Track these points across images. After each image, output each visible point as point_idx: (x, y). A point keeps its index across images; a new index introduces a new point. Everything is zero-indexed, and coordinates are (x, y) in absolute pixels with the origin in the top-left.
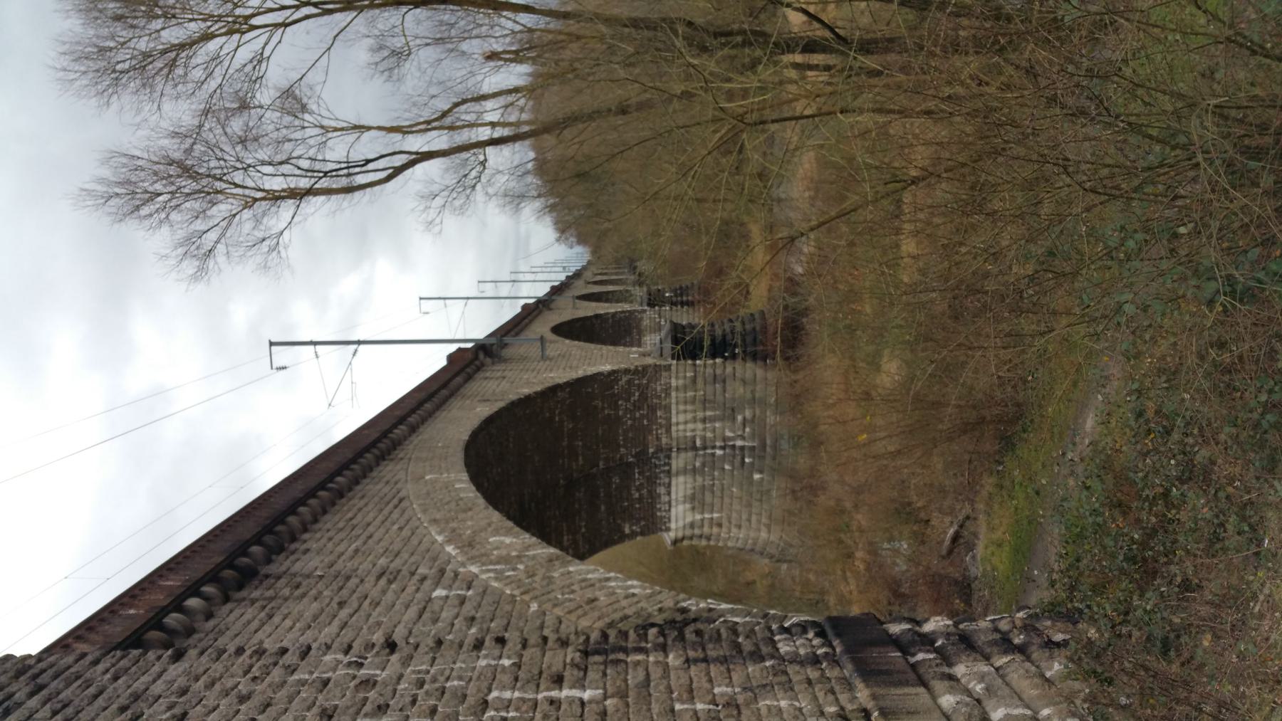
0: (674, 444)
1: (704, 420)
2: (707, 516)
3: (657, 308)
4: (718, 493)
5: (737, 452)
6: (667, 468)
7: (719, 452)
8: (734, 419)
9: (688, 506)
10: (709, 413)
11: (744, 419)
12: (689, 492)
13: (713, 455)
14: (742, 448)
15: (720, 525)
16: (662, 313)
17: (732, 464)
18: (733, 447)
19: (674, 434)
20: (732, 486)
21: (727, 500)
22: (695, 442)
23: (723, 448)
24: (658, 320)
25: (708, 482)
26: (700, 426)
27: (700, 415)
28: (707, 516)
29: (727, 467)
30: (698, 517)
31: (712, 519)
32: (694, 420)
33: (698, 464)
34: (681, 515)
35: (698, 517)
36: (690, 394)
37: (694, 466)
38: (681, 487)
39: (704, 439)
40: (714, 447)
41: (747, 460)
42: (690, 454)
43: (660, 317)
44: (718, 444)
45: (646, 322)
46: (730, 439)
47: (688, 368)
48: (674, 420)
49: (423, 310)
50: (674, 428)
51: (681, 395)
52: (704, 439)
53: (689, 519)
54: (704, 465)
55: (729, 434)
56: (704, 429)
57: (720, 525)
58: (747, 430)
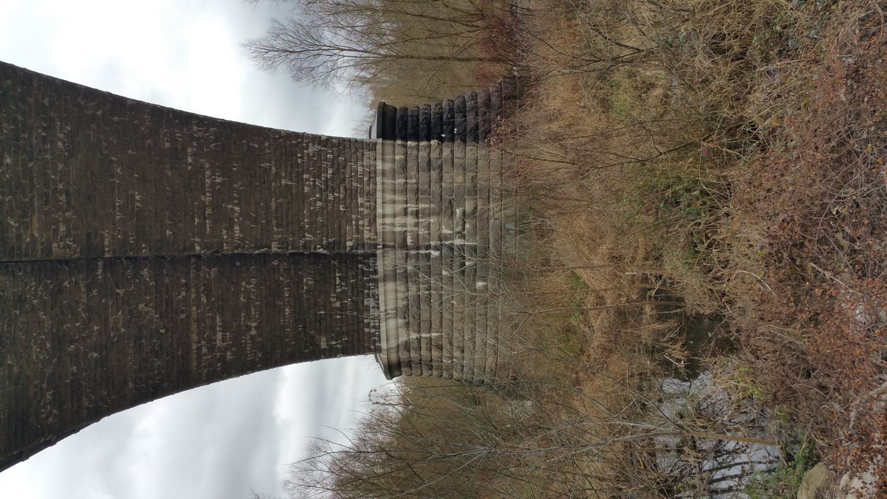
1: (417, 214)
7: (435, 253)
8: (452, 214)
9: (401, 321)
11: (464, 213)
12: (401, 304)
13: (428, 256)
15: (440, 348)
18: (451, 248)
19: (379, 228)
22: (405, 239)
26: (411, 220)
27: (412, 207)
28: (424, 335)
34: (392, 332)
39: (417, 237)
42: (400, 253)
44: (432, 243)
46: (447, 237)
48: (379, 211)
50: (379, 221)
52: (417, 237)
53: (403, 339)
55: (446, 231)
56: (417, 225)
57: (440, 348)
58: (467, 226)
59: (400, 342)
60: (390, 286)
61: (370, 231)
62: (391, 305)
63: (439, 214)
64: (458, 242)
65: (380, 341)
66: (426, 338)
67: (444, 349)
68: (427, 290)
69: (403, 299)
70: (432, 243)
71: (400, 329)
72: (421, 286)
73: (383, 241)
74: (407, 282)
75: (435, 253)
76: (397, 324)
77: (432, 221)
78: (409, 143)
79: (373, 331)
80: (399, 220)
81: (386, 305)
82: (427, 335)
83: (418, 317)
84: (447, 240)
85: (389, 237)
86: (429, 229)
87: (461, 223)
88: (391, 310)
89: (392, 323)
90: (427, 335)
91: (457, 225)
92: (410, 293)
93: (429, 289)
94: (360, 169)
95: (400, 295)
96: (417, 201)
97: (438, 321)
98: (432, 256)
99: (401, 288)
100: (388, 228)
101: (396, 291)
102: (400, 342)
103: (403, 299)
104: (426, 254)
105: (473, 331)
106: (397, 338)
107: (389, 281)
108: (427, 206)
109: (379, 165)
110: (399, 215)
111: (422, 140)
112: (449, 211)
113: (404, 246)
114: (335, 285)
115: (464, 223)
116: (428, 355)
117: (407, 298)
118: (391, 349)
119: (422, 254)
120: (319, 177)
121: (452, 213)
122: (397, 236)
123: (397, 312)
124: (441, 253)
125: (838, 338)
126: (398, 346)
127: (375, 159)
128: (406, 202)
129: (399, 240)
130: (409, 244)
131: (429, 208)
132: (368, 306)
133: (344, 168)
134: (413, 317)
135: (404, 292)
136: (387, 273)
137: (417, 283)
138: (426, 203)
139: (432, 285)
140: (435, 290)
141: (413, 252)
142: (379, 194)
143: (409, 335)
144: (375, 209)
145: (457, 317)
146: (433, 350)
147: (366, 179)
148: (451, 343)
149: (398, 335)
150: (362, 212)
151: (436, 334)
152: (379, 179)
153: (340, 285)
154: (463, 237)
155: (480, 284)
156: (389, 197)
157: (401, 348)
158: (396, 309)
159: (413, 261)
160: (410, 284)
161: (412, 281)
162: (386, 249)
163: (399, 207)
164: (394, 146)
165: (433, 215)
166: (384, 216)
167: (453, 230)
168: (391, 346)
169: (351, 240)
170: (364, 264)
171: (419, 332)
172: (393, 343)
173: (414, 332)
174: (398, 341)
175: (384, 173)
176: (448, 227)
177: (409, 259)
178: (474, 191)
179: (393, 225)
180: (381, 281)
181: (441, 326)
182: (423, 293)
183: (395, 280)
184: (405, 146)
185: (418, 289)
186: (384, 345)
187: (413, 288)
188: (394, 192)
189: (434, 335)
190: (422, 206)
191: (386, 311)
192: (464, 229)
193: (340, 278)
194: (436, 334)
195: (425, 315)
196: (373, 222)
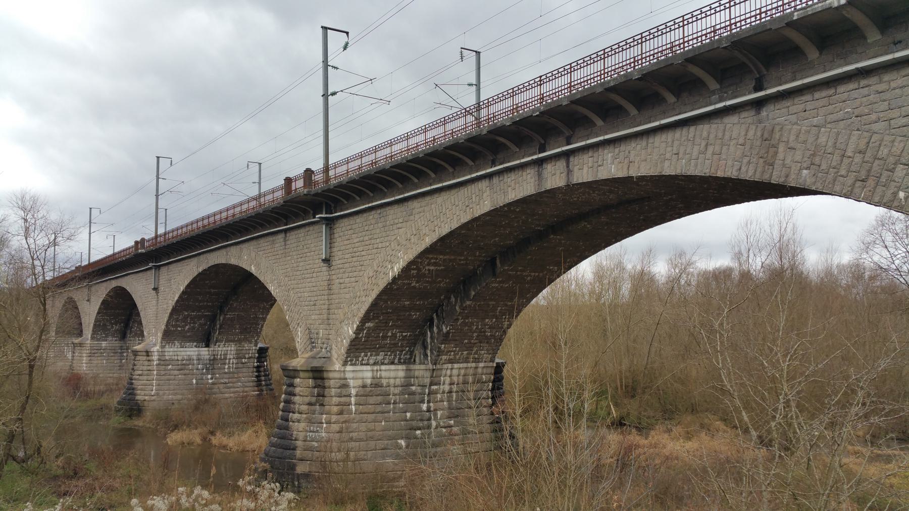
0: (438, 366)
1: (450, 392)
2: (353, 400)
3: (257, 355)
4: (379, 409)
5: (426, 423)
6: (396, 361)
7: (424, 407)
8: (449, 418)
9: (369, 381)
10: (454, 395)
11: (451, 427)
12: (384, 382)
13: (422, 402)
14: (429, 427)
15: (341, 413)
16: (252, 360)
17: (412, 419)
18: (429, 419)
19: (445, 366)
20: (386, 421)
21: (371, 417)
22: (436, 384)
23: (429, 410)
24: (247, 356)
25: (392, 398)
26: (447, 388)
27: (455, 388)
28: (353, 400)
29: (408, 415)
30: (353, 392)
31: (350, 404)
32: (451, 384)
33: (413, 388)
34: (360, 375)
35: (353, 392)
36: (471, 379)
37: (413, 385)
38: (392, 374)
39: (436, 392)
40: (429, 402)
41: (418, 432)
42: (427, 381)
43: (249, 358)
44: (431, 404)
45: (246, 346)
46: (435, 415)
47: (488, 376)
48: (456, 366)
49: (251, 165)
50: (450, 366)
51: (471, 371)
52: (436, 392)
53: (351, 383)
54: (413, 393)
55: (439, 413)
56: (443, 392)
57: (341, 413)
58: (444, 430)
59: (349, 380)
60: (401, 374)
61: (445, 360)
62: (384, 374)
63: (450, 408)
64: (434, 423)
65: (352, 365)
66: (351, 401)
67: (339, 416)
68: (394, 401)
69: (388, 383)
70: (431, 404)
71: (361, 380)
72: (398, 397)
73: (438, 369)
74: (401, 386)
75: (424, 407)
76: (366, 378)
77: (445, 403)
78: (491, 384)
79: (360, 359)
80: (448, 380)
81: (385, 370)
82: (353, 403)
83: (370, 394)
84: (434, 415)
85: (439, 373)
86: (440, 401)
87: (446, 425)
88: (380, 374)
89: (369, 375)
90: (353, 403)
91: (444, 422)
92: (392, 389)
93: (395, 403)
94: (483, 352)
95: (392, 381)
96: (457, 392)
97: (366, 410)
98: (422, 404)
99: (398, 382)
100: (444, 372)
101: (395, 378)
102: (349, 380)
103: (388, 383)
104: (424, 400)
105: (360, 440)
106: (353, 378)
107: (406, 373)
108: (454, 399)
109: (481, 365)
110: (451, 379)
111: (492, 393)
112: (452, 415)
113: (431, 384)
114: (402, 332)
115: (445, 427)
116: (333, 403)
117: (389, 386)
118: (345, 374)
119: (424, 397)
120: (489, 328)
121: (450, 418)
122: (438, 379)
123: (377, 378)
124: (424, 411)
125: (883, 460)
126: (346, 379)
127: (485, 362)
128: (458, 384)
129: (436, 380)
130: (432, 387)
131: (453, 401)
132: (378, 355)
133: (487, 343)
134: (371, 391)
135: (395, 384)
136: (413, 371)
137: (402, 393)
138: (456, 399)
139: (397, 405)
140: (394, 408)
141: (427, 391)
142: (465, 365)
143: (354, 387)
144: (458, 363)
145: (371, 426)
146: (338, 407)
147: (476, 356)
148: (345, 422)
149: (356, 379)
150: (458, 354)
151: (354, 409)
152: (474, 365)
153: (402, 335)
154: (437, 427)
155: (402, 442)
156: (463, 372)
157: (342, 382)
158: (381, 378)
159: (420, 391)
160: (400, 389)
161: (403, 390)
162: (431, 371)
163: (455, 379)
164: (490, 374)
165: (449, 404)
166: (452, 369)
167: (440, 419)
168: (346, 373)
169: (445, 347)
170: (407, 352)
171: (356, 396)
172: (349, 375)
173: (357, 392)
174: (350, 379)
175: (476, 368)
176: (442, 415)
177: (421, 387)
178: (465, 432)
179: (445, 375)
180: (406, 367)
181: (361, 413)
182: (392, 398)
183: (405, 378)
184: (489, 381)
185: (395, 395)
186: (349, 368)
187: (397, 390)
188: (465, 375)
189: (155, 372)
190: (454, 395)
191: (380, 370)
192: (442, 427)
193: (406, 336)
194: (354, 409)
195: (372, 400)
196: (451, 361)
